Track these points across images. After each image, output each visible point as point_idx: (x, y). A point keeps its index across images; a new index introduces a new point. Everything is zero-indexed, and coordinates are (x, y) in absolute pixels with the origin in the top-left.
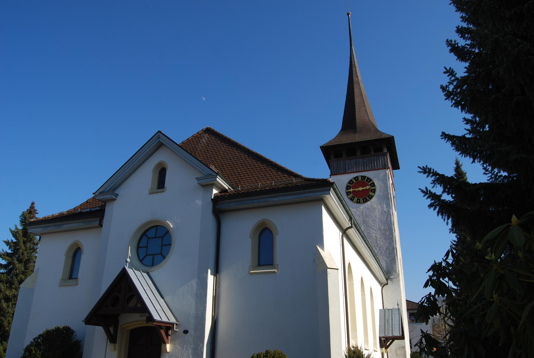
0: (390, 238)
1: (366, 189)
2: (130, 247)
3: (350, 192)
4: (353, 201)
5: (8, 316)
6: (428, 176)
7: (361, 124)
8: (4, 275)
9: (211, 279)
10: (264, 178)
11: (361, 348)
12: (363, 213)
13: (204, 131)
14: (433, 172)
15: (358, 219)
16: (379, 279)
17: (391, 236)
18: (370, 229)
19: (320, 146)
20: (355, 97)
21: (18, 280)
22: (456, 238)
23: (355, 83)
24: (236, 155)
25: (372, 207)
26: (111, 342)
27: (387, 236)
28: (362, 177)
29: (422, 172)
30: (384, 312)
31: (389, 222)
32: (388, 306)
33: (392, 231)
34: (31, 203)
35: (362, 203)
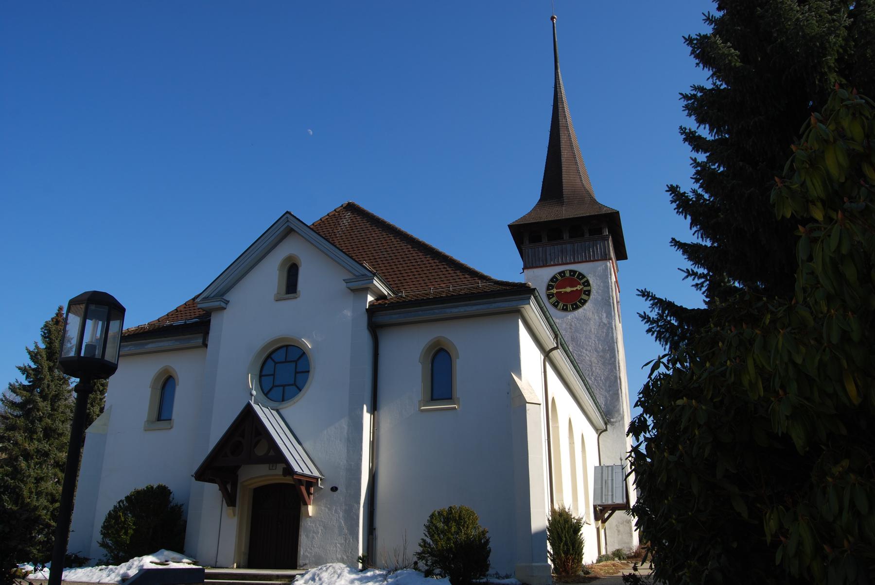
0: (611, 362)
1: (577, 289)
2: (250, 375)
3: (553, 293)
4: (557, 307)
5: (30, 482)
6: (646, 300)
7: (570, 191)
8: (20, 419)
9: (367, 418)
10: (436, 280)
11: (569, 509)
12: (571, 325)
13: (344, 208)
14: (652, 296)
15: (566, 335)
16: (595, 422)
17: (613, 359)
18: (581, 350)
19: (509, 224)
20: (561, 149)
21: (43, 426)
23: (562, 127)
24: (394, 244)
25: (584, 316)
26: (228, 506)
27: (606, 359)
28: (571, 271)
29: (641, 295)
30: (600, 470)
31: (610, 338)
32: (606, 462)
33: (615, 352)
34: (58, 308)
35: (570, 310)
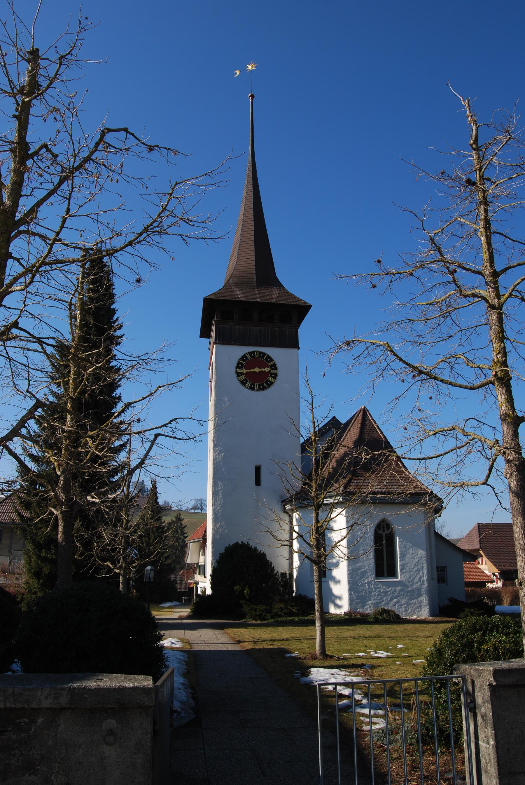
28: (260, 353)
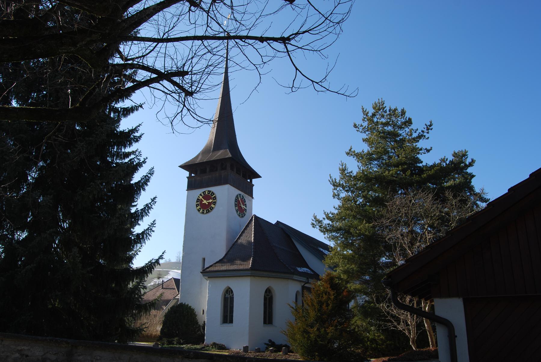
22: (266, 345)
28: (208, 191)
